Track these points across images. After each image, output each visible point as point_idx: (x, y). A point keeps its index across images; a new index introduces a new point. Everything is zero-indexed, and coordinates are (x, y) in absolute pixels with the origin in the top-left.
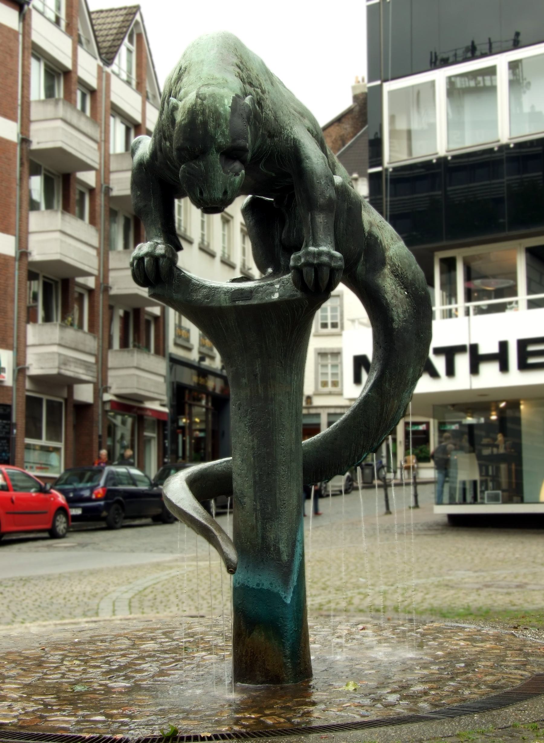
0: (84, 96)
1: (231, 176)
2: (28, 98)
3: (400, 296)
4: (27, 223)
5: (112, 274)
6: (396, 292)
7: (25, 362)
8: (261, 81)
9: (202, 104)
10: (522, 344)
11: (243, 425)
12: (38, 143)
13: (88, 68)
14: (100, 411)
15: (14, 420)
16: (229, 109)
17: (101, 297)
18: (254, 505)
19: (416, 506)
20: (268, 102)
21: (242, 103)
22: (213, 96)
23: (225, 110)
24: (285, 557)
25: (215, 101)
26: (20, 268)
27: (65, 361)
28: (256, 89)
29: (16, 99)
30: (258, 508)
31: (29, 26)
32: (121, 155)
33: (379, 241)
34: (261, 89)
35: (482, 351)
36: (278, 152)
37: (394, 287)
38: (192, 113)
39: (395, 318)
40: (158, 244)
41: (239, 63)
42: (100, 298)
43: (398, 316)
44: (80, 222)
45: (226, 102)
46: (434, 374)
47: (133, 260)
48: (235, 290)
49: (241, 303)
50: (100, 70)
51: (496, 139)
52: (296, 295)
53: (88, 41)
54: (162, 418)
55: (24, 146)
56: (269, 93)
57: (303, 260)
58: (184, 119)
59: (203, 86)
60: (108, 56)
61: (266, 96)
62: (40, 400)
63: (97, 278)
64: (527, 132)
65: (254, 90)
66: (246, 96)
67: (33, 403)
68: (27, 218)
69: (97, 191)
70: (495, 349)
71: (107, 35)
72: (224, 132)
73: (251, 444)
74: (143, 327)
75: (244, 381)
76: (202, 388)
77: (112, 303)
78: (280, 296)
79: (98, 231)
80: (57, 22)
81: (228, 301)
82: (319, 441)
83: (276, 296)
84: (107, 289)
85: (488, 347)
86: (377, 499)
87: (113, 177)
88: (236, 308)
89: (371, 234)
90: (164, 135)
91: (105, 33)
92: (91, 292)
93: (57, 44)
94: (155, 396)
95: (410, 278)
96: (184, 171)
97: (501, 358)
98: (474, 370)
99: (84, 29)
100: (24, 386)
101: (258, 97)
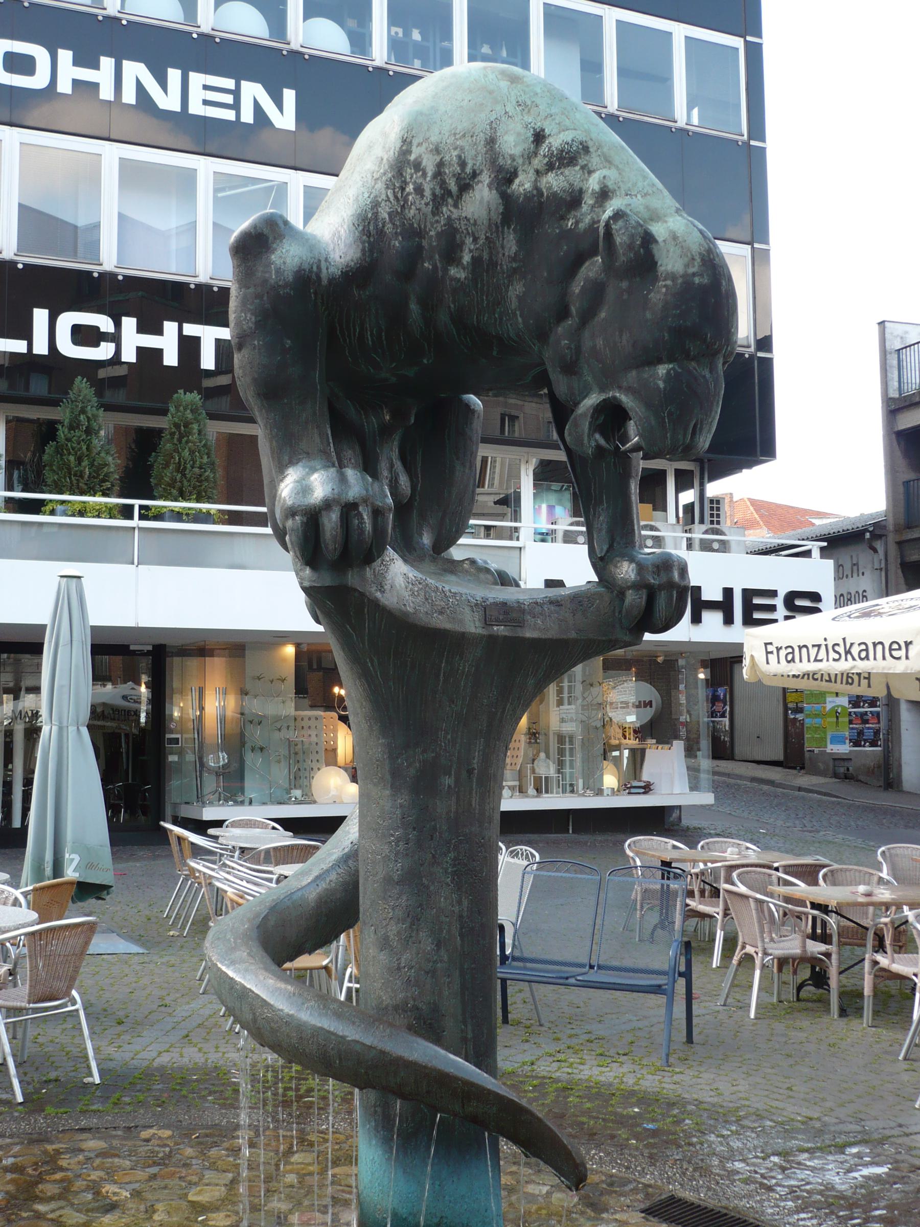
10: (748, 594)
18: (462, 1031)
30: (470, 1035)
35: (706, 596)
49: (500, 630)
70: (719, 597)
73: (456, 909)
81: (477, 624)
85: (712, 593)
86: (390, 531)
97: (725, 606)
98: (696, 619)
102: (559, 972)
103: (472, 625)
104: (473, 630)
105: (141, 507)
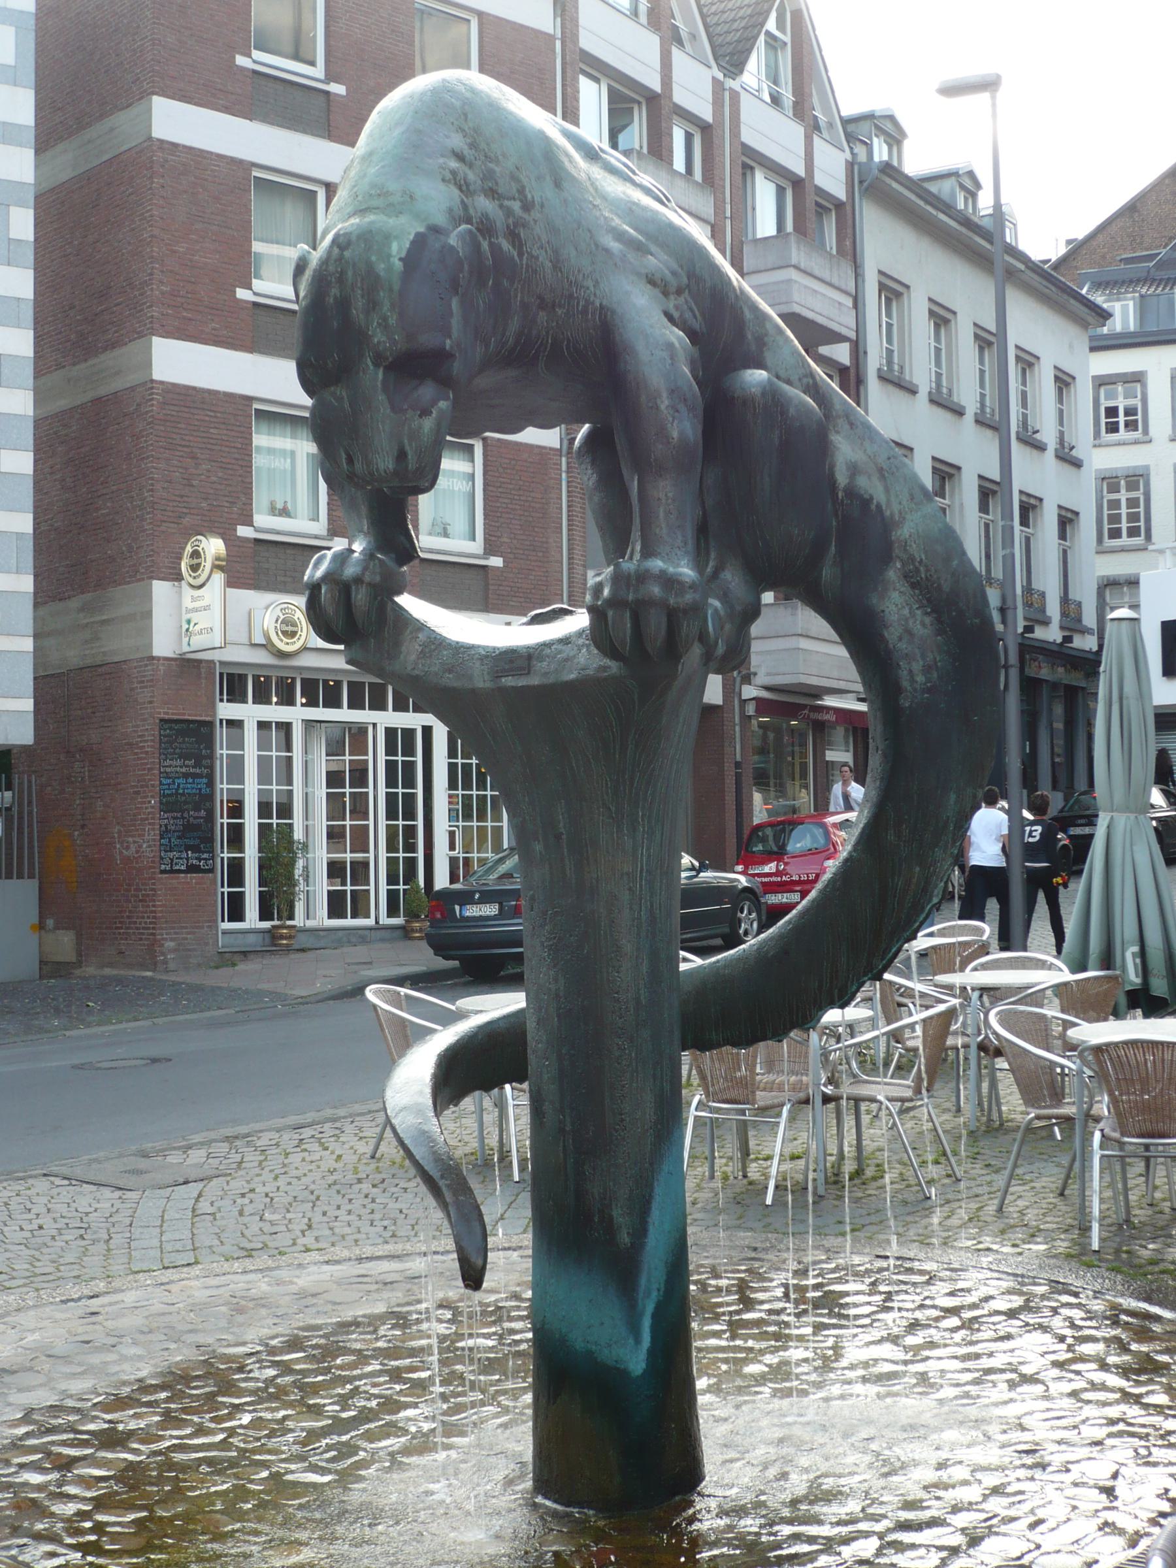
0: (689, 138)
3: (918, 629)
6: (911, 622)
8: (525, 181)
9: (340, 259)
13: (693, 84)
16: (398, 265)
23: (389, 269)
24: (624, 1238)
28: (506, 203)
33: (873, 507)
36: (569, 340)
37: (906, 612)
39: (905, 684)
43: (913, 681)
45: (395, 247)
48: (500, 654)
49: (508, 681)
50: (718, 87)
52: (609, 667)
53: (694, 37)
56: (542, 206)
60: (732, 59)
65: (501, 206)
66: (467, 223)
71: (734, 20)
72: (385, 319)
75: (538, 847)
82: (739, 959)
88: (502, 690)
89: (851, 492)
94: (842, 685)
95: (946, 587)
101: (510, 221)
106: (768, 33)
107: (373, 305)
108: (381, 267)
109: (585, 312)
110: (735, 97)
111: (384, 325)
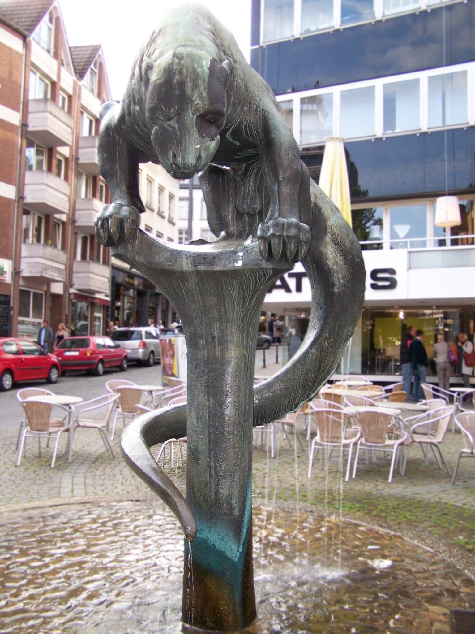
1: (206, 141)
2: (27, 97)
4: (24, 179)
5: (77, 213)
7: (19, 268)
11: (199, 384)
12: (33, 127)
13: (67, 80)
14: (67, 299)
15: (12, 305)
16: (207, 71)
17: (70, 227)
18: (208, 462)
19: (264, 367)
20: (239, 72)
21: (218, 66)
22: (191, 56)
23: (203, 71)
25: (193, 61)
26: (18, 207)
27: (46, 268)
29: (20, 97)
31: (30, 51)
32: (86, 137)
34: (233, 58)
38: (169, 72)
39: (336, 283)
40: (122, 205)
41: (213, 30)
42: (69, 228)
44: (58, 179)
45: (204, 63)
46: (288, 290)
47: (98, 221)
49: (201, 268)
50: (75, 84)
51: (465, 122)
53: (68, 64)
54: (106, 304)
55: (24, 128)
57: (271, 231)
58: (160, 78)
59: (179, 46)
60: (80, 74)
61: (237, 66)
62: (29, 293)
63: (68, 215)
64: (456, 123)
67: (24, 294)
68: (24, 175)
69: (70, 159)
72: (201, 93)
74: (96, 246)
76: (132, 285)
77: (76, 231)
78: (244, 264)
79: (70, 185)
80: (49, 51)
81: (190, 265)
83: (239, 264)
84: (74, 222)
87: (81, 151)
88: (198, 272)
89: (316, 205)
90: (134, 98)
91: (79, 60)
92: (64, 223)
93: (49, 65)
95: (348, 246)
96: (156, 133)
99: (65, 55)
100: (19, 283)
102: (178, 401)
103: (186, 266)
104: (187, 268)
105: (411, 242)
106: (92, 69)
107: (195, 86)
108: (199, 70)
109: (256, 110)
110: (80, 88)
111: (200, 96)
